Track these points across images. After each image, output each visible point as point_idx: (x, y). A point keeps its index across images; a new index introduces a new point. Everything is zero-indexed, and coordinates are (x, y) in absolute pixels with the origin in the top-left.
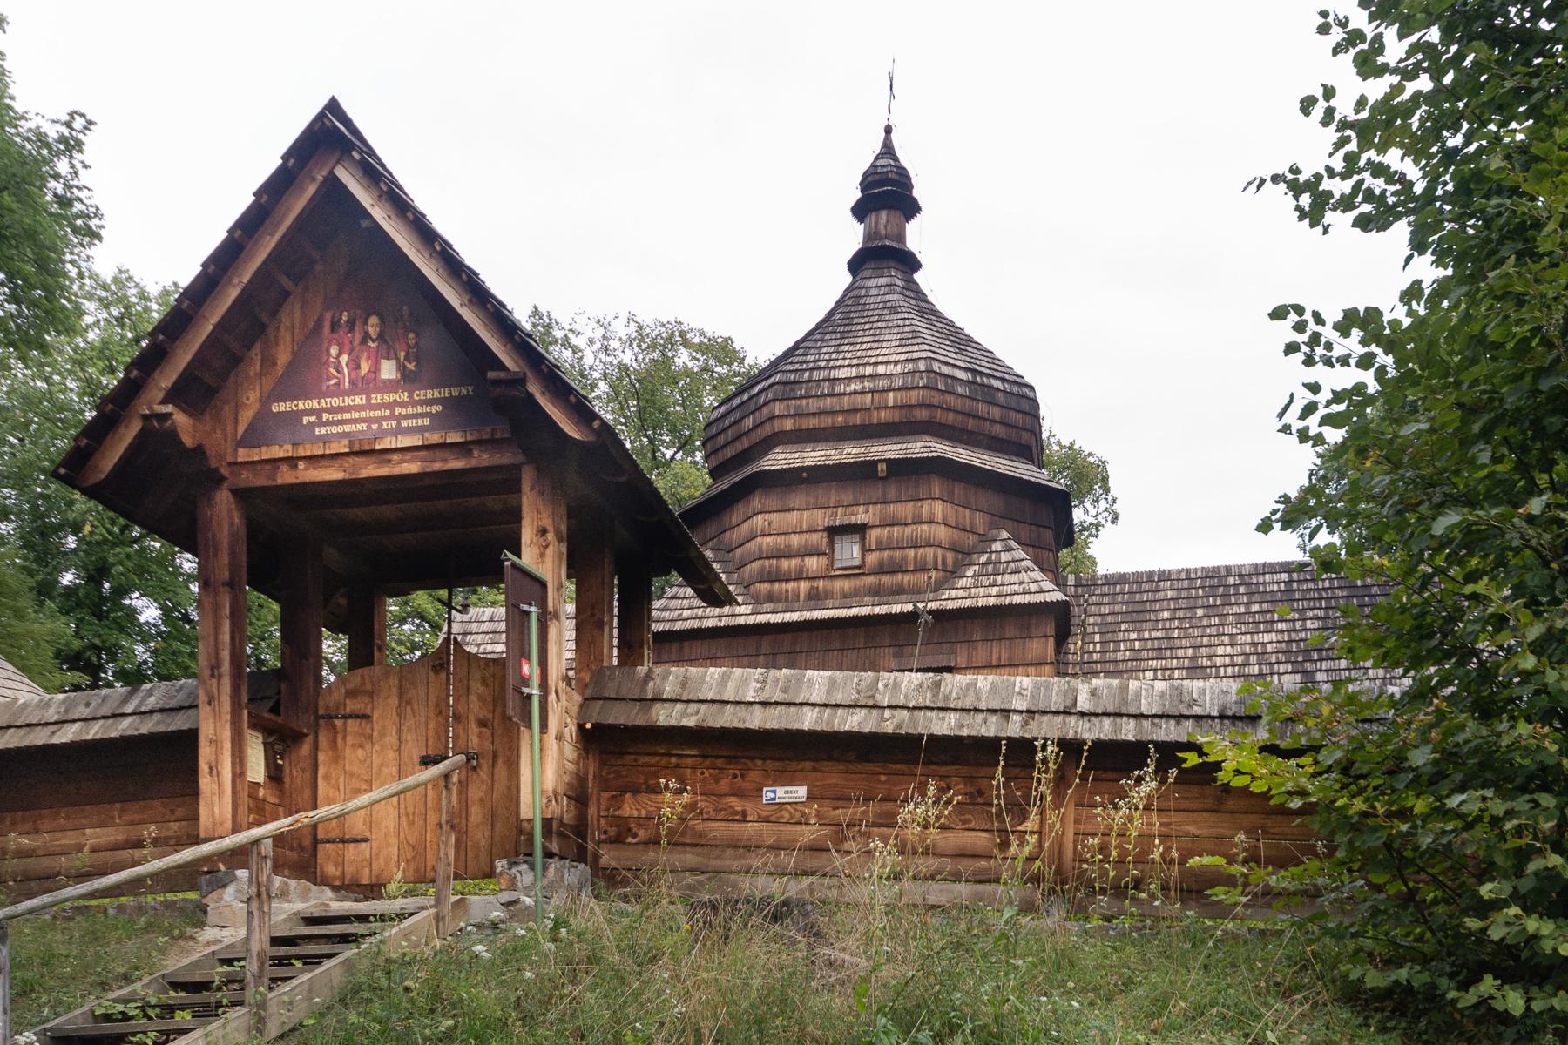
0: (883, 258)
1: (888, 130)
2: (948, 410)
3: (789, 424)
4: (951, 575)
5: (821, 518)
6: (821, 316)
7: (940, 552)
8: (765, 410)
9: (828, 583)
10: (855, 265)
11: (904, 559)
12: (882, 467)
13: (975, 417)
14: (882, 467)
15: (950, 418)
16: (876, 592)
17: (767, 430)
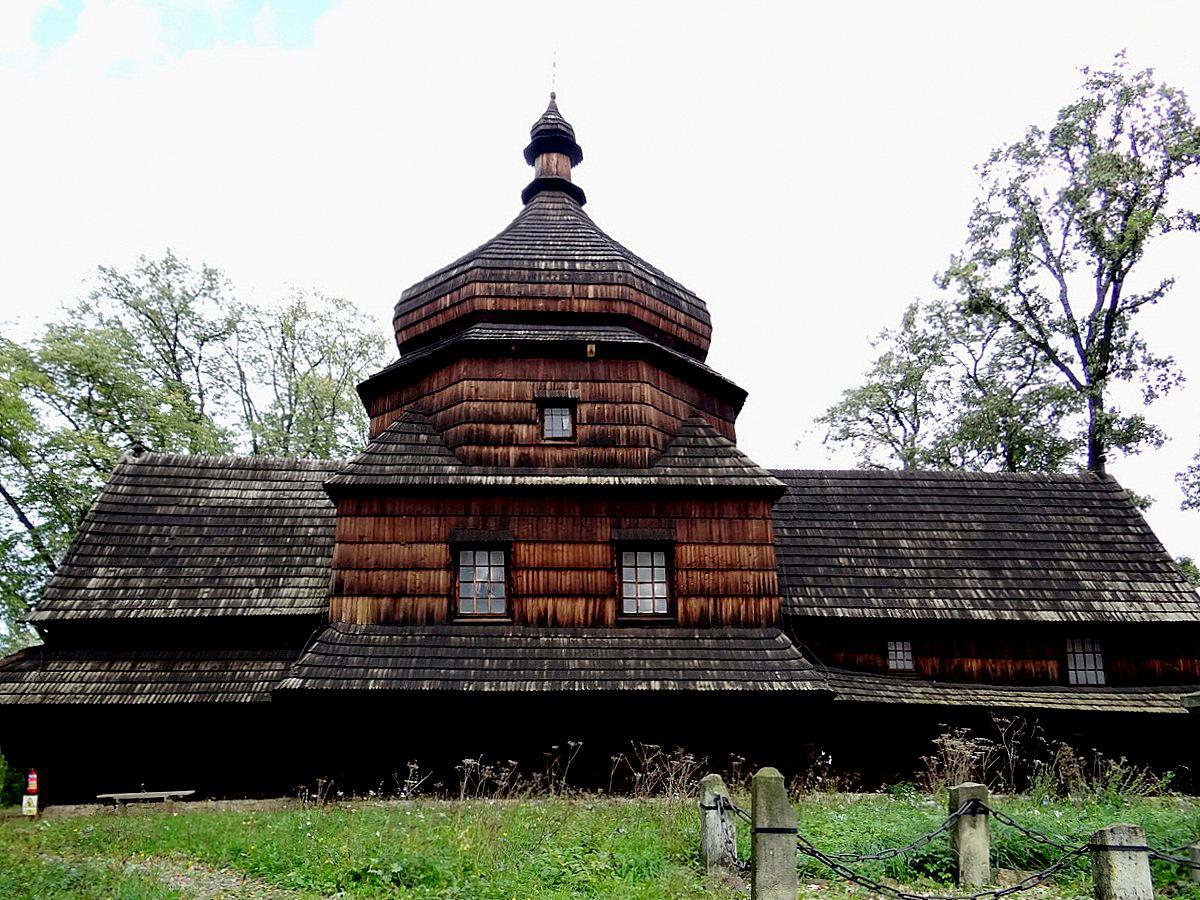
1: (553, 96)
2: (644, 308)
3: (489, 304)
4: (664, 452)
5: (529, 388)
6: (510, 221)
7: (651, 432)
8: (464, 290)
9: (539, 451)
10: (529, 195)
11: (617, 434)
12: (591, 348)
13: (665, 318)
14: (591, 348)
15: (645, 316)
17: (467, 307)
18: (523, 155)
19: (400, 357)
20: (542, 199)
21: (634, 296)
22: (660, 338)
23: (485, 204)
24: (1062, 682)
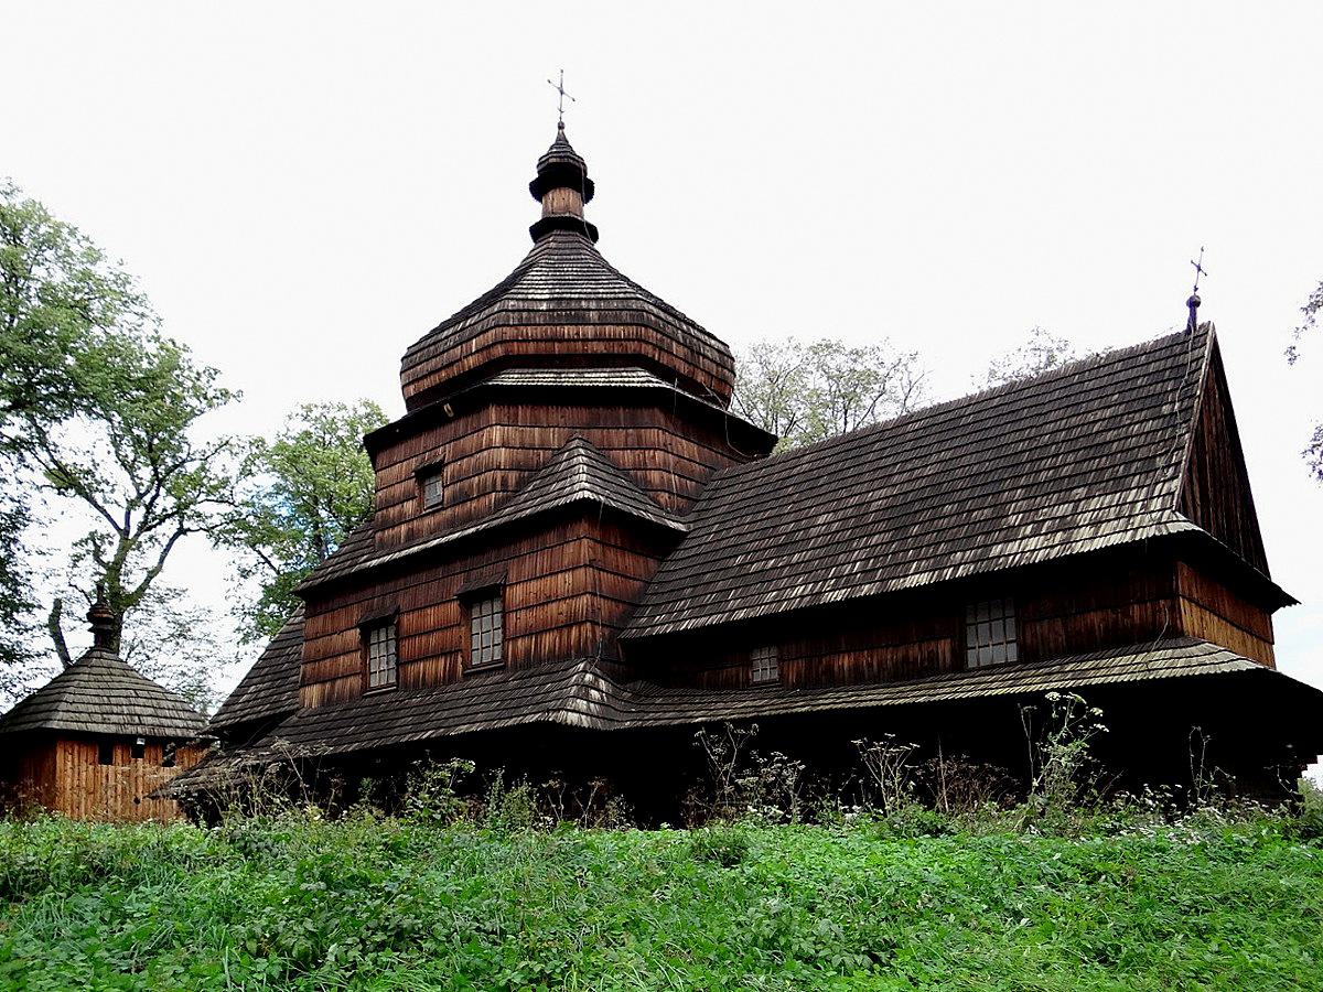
0: (563, 231)
1: (561, 127)
2: (526, 341)
7: (499, 474)
10: (537, 232)
13: (561, 340)
15: (531, 348)
16: (453, 524)
18: (529, 193)
19: (405, 412)
20: (552, 241)
21: (509, 332)
22: (681, 382)
23: (493, 241)
24: (959, 666)
